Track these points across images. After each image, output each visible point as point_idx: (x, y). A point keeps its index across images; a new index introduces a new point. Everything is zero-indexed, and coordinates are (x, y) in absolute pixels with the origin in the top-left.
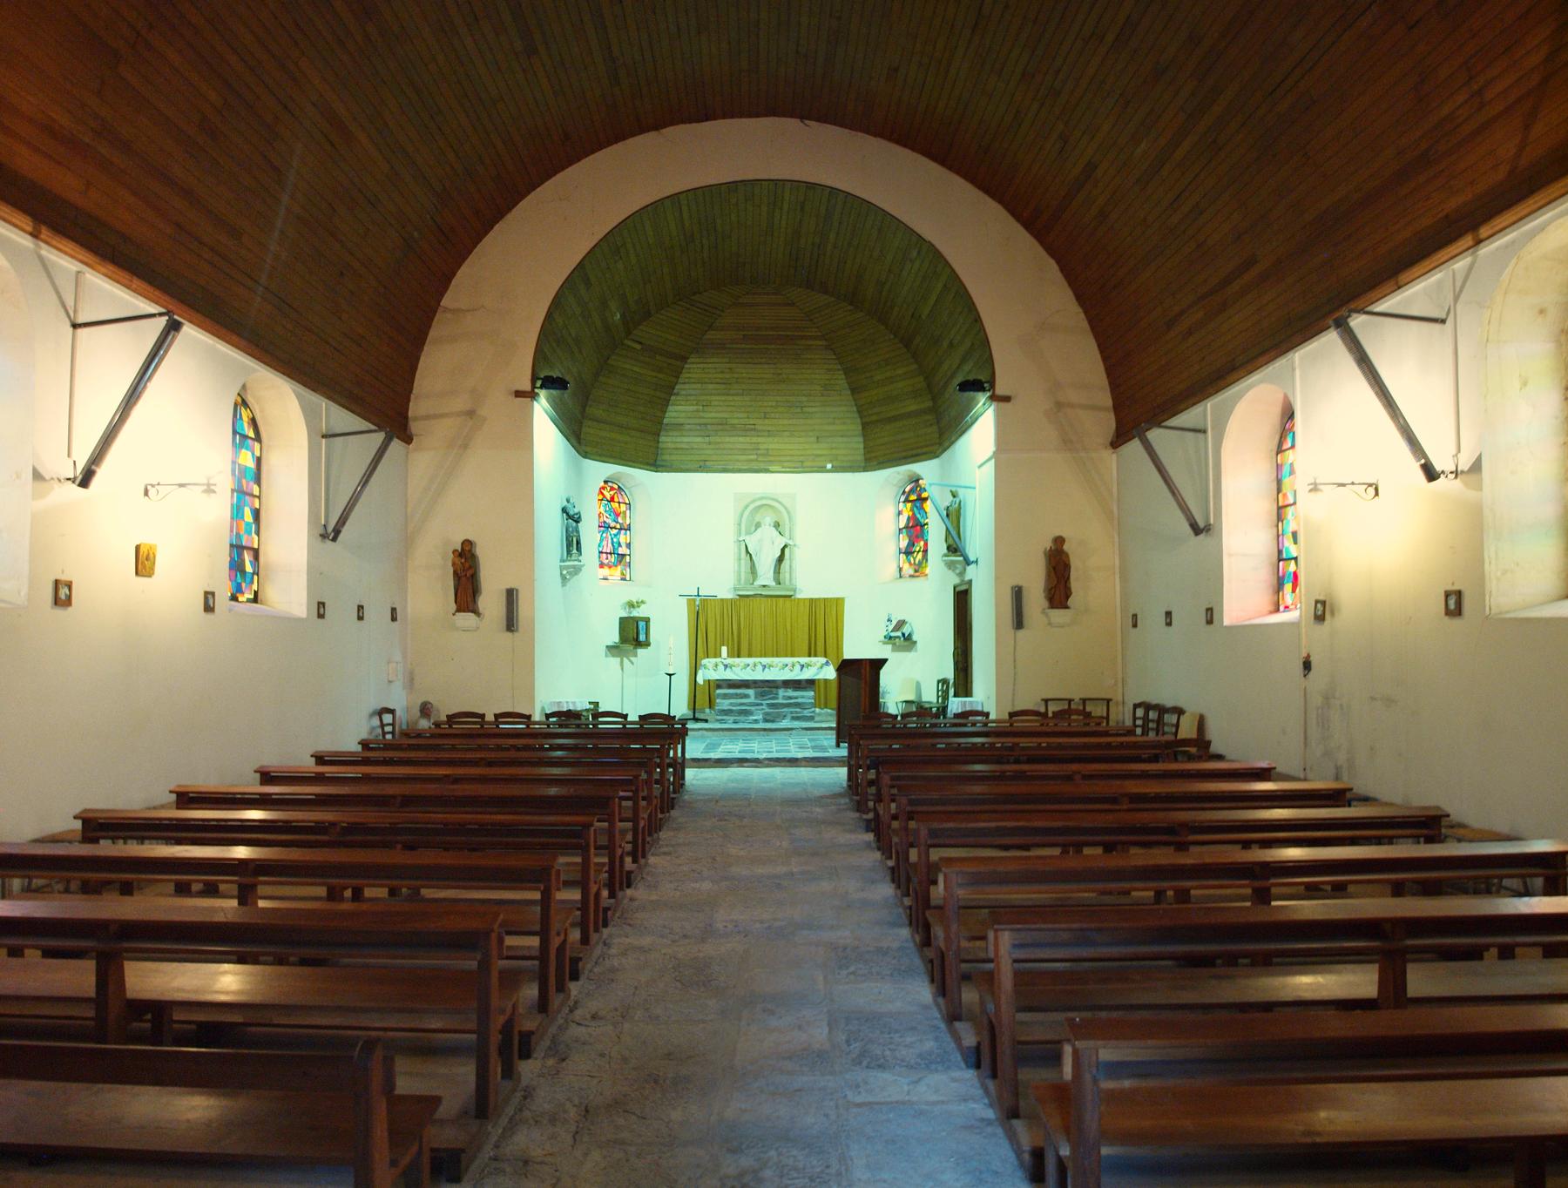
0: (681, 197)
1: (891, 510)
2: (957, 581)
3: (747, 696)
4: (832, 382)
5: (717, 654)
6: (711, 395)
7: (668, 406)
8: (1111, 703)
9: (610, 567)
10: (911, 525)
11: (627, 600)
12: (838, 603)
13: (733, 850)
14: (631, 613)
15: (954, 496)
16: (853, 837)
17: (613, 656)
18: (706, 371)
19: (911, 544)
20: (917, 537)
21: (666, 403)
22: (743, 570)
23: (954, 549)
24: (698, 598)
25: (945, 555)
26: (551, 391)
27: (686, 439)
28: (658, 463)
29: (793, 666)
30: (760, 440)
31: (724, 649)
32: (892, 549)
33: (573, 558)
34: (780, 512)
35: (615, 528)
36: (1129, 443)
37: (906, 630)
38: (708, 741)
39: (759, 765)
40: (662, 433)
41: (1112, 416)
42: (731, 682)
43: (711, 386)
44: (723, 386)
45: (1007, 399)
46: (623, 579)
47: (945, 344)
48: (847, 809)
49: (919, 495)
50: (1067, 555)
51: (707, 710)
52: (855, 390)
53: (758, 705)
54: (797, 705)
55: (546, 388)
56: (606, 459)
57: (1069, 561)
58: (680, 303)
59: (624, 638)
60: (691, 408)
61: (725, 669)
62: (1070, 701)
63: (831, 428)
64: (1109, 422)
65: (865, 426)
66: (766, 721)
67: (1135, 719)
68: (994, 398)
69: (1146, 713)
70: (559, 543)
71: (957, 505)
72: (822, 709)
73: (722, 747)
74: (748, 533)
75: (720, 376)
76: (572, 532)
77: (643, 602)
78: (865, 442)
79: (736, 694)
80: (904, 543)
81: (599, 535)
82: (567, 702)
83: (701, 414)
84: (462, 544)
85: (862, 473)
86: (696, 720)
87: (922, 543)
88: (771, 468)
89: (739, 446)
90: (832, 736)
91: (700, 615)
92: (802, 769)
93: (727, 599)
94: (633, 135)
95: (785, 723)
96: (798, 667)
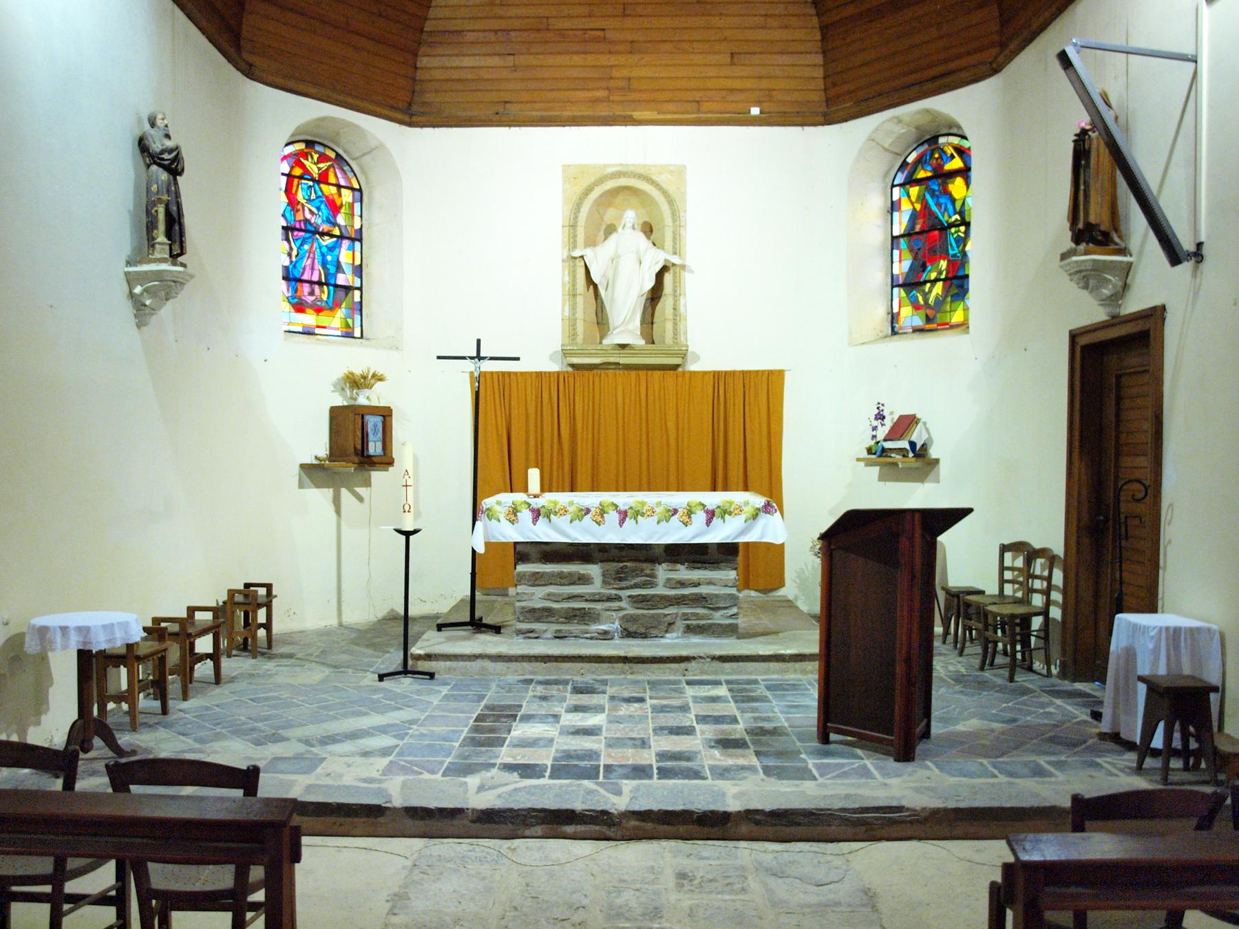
1: (876, 202)
3: (584, 580)
5: (514, 483)
9: (318, 310)
10: (918, 228)
11: (340, 373)
17: (318, 486)
19: (920, 265)
20: (932, 250)
22: (580, 314)
27: (467, 62)
28: (415, 108)
29: (690, 513)
30: (613, 60)
31: (534, 475)
32: (878, 278)
37: (918, 436)
40: (423, 50)
46: (349, 335)
53: (609, 599)
54: (700, 600)
59: (337, 452)
61: (535, 520)
63: (761, 35)
65: (825, 31)
66: (628, 634)
74: (591, 242)
77: (724, 521)
78: (825, 65)
79: (561, 575)
80: (902, 267)
88: (637, 115)
89: (575, 73)
95: (672, 643)
96: (700, 517)
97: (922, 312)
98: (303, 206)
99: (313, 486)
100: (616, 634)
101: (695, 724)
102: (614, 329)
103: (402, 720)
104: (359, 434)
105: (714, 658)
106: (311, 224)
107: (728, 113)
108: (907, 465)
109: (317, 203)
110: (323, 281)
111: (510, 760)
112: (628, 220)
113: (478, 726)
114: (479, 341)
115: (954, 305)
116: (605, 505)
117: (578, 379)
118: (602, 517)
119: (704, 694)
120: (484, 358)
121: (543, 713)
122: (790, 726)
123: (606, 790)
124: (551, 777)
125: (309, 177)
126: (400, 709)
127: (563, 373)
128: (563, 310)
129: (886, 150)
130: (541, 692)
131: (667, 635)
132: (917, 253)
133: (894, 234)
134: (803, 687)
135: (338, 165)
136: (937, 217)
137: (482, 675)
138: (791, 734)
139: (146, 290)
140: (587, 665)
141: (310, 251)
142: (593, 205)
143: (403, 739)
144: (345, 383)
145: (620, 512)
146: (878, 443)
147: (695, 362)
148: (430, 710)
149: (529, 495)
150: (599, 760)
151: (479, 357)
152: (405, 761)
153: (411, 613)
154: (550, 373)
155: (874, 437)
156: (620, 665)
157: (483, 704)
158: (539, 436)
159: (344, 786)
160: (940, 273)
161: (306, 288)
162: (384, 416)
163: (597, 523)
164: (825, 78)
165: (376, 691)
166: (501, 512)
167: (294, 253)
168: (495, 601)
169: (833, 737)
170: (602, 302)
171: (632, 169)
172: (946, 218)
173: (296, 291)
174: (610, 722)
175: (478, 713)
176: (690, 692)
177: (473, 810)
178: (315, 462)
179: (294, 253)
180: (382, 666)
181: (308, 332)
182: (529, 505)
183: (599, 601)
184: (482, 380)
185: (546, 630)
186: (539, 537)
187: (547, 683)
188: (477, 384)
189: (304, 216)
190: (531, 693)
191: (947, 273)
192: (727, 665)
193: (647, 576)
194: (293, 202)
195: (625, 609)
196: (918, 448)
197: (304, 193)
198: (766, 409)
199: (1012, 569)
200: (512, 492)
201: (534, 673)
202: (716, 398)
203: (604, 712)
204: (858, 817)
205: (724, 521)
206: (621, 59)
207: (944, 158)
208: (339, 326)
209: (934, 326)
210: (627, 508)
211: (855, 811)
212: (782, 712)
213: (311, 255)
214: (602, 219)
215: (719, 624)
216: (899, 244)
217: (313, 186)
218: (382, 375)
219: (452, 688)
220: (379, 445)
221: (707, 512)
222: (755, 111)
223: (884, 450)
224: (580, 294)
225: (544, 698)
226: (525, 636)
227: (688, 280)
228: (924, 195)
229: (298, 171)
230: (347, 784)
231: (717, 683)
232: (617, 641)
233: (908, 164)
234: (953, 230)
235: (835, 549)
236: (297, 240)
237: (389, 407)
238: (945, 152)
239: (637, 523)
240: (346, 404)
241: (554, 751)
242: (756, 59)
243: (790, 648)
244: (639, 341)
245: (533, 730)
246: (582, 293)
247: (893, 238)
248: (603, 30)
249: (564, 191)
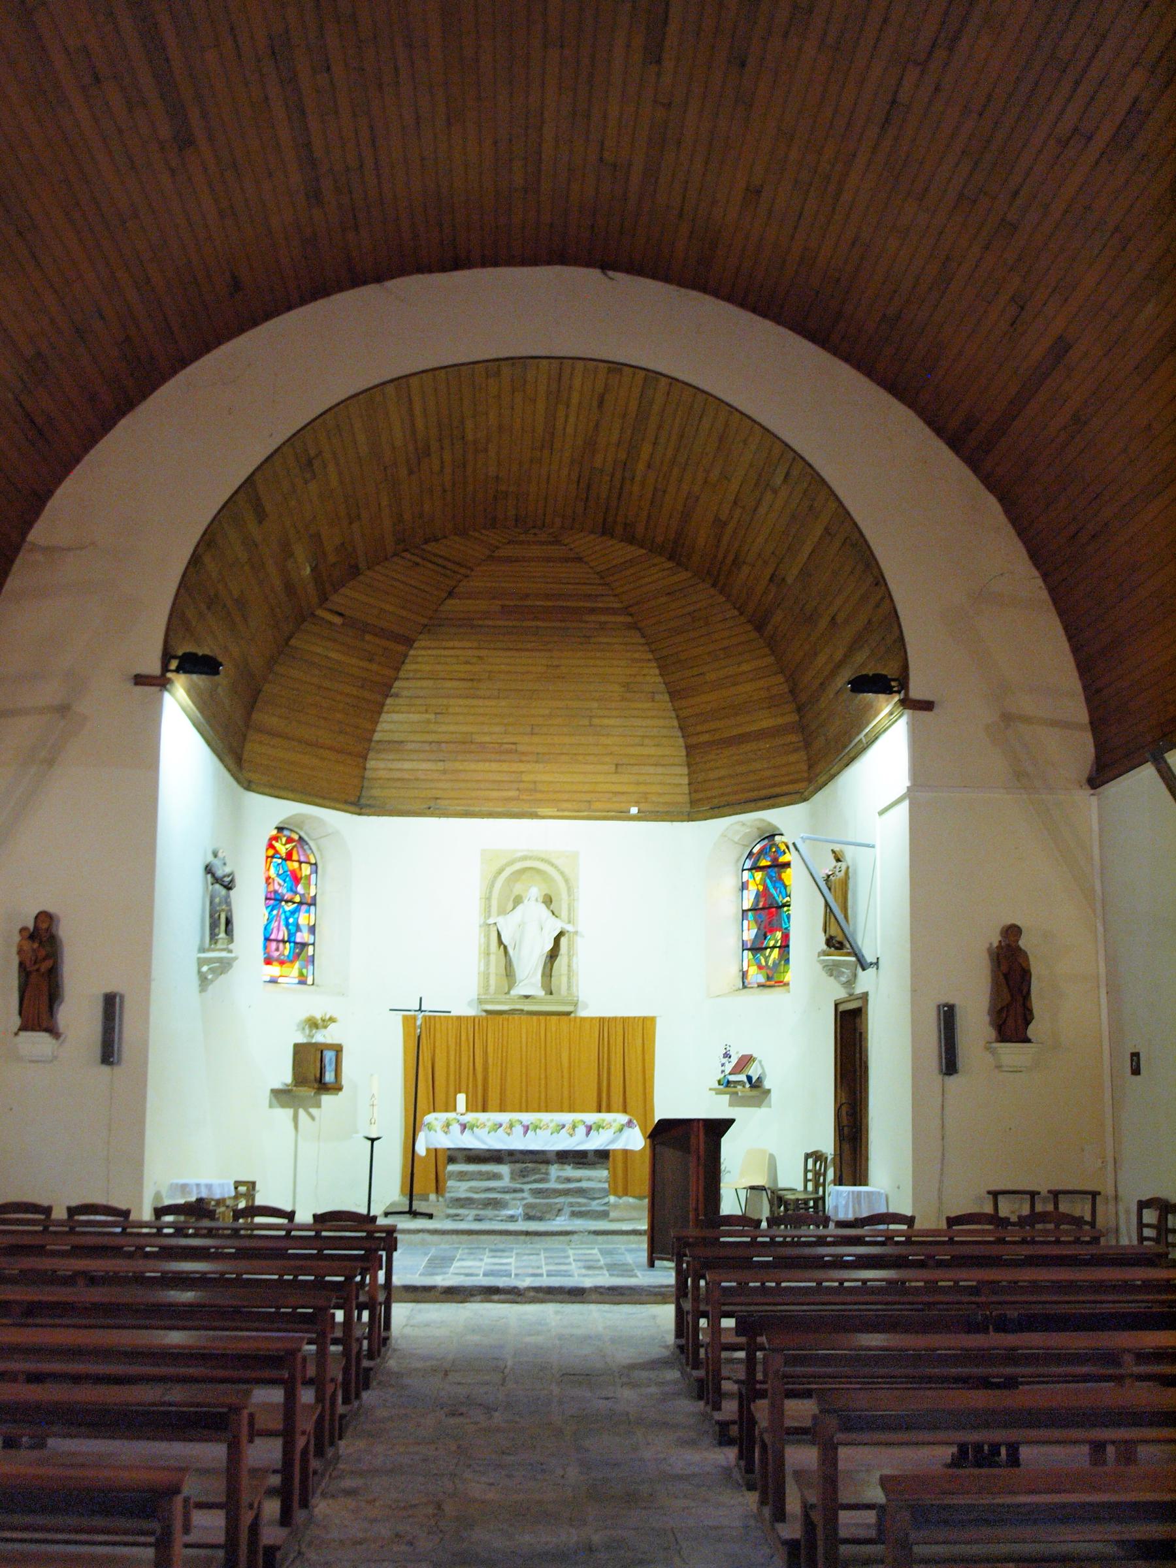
0: (414, 381)
1: (730, 882)
2: (842, 994)
3: (496, 1176)
4: (639, 679)
5: (450, 1107)
6: (448, 697)
7: (380, 713)
8: (1098, 1197)
9: (282, 963)
10: (761, 905)
11: (304, 1015)
12: (645, 1026)
13: (478, 1487)
14: (313, 1037)
15: (838, 860)
16: (697, 1457)
17: (283, 1106)
18: (443, 660)
19: (763, 934)
21: (379, 709)
22: (493, 969)
23: (838, 943)
24: (420, 1015)
25: (824, 953)
26: (194, 677)
27: (407, 765)
28: (363, 801)
29: (574, 1127)
30: (523, 767)
31: (461, 1098)
32: (731, 944)
33: (219, 946)
35: (291, 901)
36: (1137, 770)
38: (433, 1252)
39: (519, 1299)
40: (371, 755)
41: (1087, 739)
42: (471, 1153)
43: (449, 684)
44: (469, 684)
45: (926, 706)
46: (303, 982)
47: (823, 623)
48: (678, 1394)
49: (775, 860)
50: (1025, 955)
51: (433, 1197)
52: (675, 694)
53: (515, 1191)
54: (581, 1192)
55: (186, 672)
56: (282, 793)
57: (1029, 965)
58: (404, 554)
59: (299, 1078)
60: (415, 717)
61: (463, 1131)
62: (1033, 1195)
63: (640, 750)
64: (1084, 747)
65: (689, 748)
66: (528, 1218)
67: (1141, 1225)
68: (907, 703)
69: (1163, 1219)
70: (198, 928)
71: (843, 873)
72: (620, 1197)
73: (456, 1264)
74: (502, 912)
76: (220, 904)
77: (332, 1020)
78: (689, 775)
79: (480, 1173)
80: (750, 934)
81: (266, 913)
82: (198, 1185)
83: (432, 727)
84: (36, 917)
85: (685, 823)
86: (413, 1213)
87: (779, 935)
88: (541, 811)
90: (643, 1244)
91: (423, 1041)
92: (593, 1307)
93: (467, 1018)
94: (341, 289)
95: (560, 1223)
96: (581, 1130)
97: (764, 971)
98: (273, 880)
104: (318, 1064)
117: (490, 1022)
131: (558, 1218)
139: (209, 969)
140: (498, 1238)
141: (278, 915)
145: (524, 1126)
154: (467, 1017)
160: (777, 942)
164: (689, 784)
166: (438, 1126)
170: (510, 960)
181: (273, 981)
206: (529, 767)
209: (772, 983)
214: (512, 891)
215: (597, 1211)
220: (333, 1074)
222: (634, 810)
223: (728, 1082)
227: (580, 943)
242: (635, 769)
244: (541, 993)
247: (744, 911)
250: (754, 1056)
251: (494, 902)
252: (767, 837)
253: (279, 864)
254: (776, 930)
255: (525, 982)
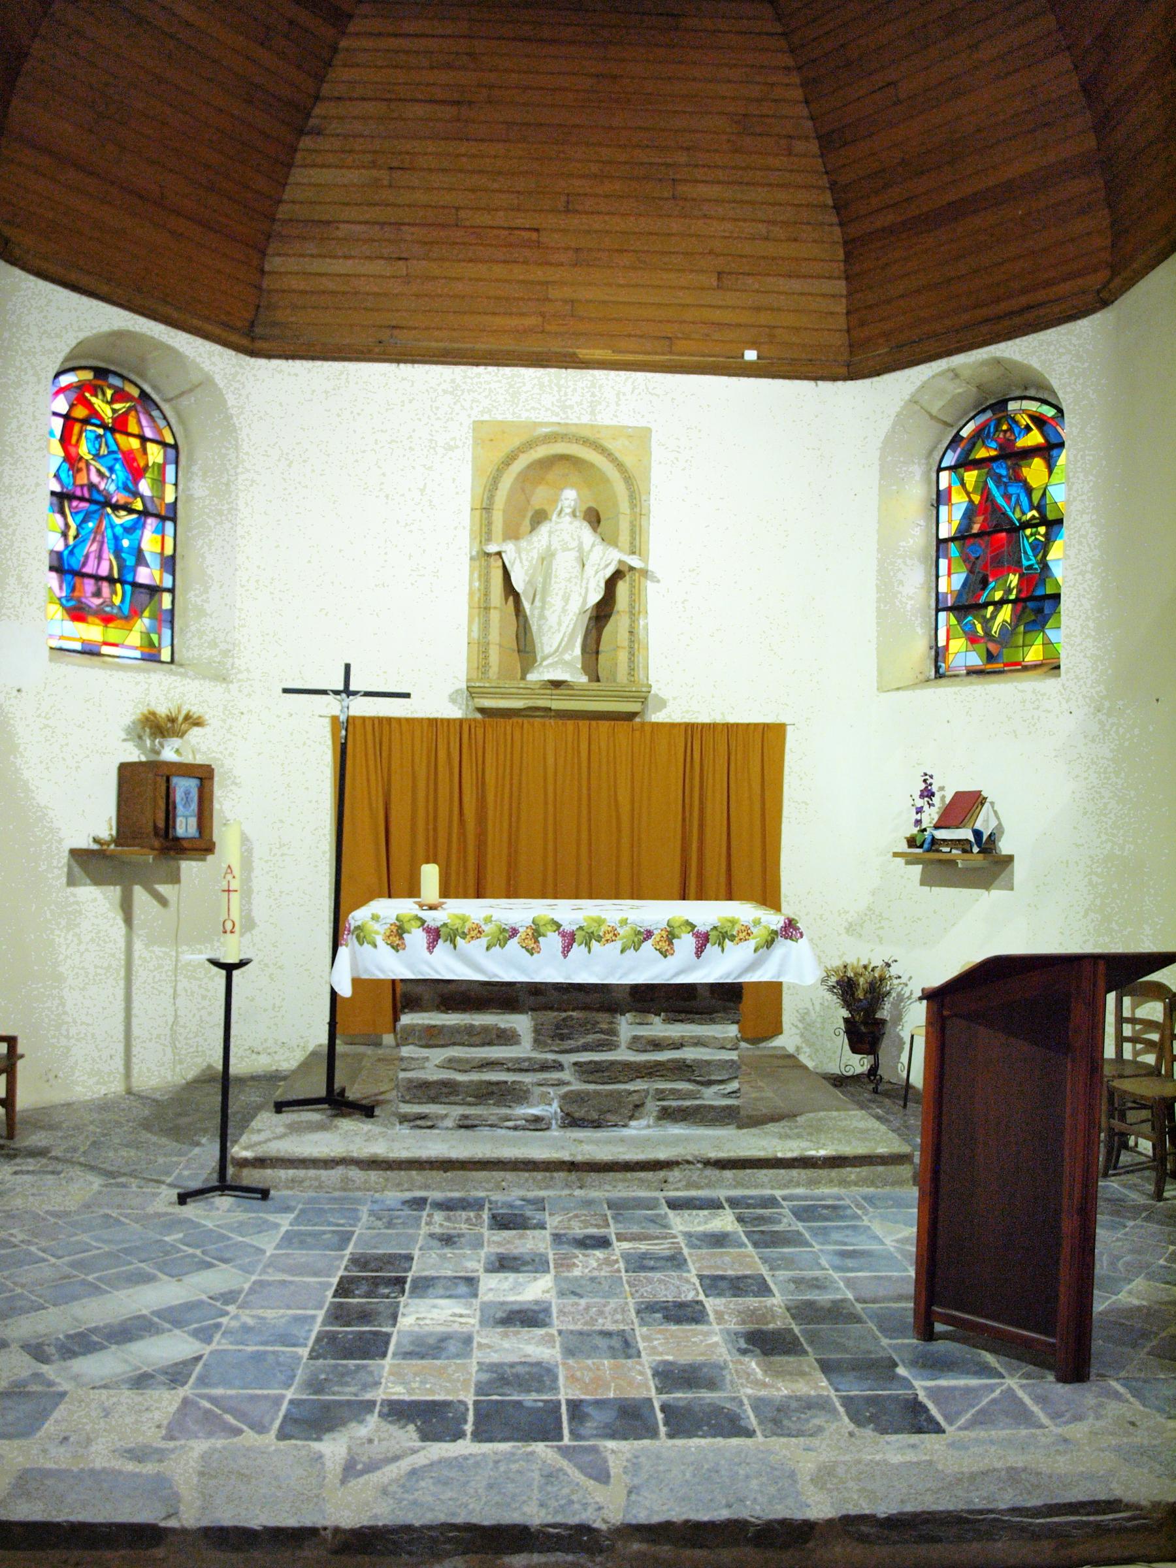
1: (916, 492)
3: (506, 1037)
9: (107, 620)
10: (976, 528)
19: (978, 580)
22: (494, 636)
28: (258, 330)
29: (671, 936)
31: (430, 874)
34: (605, 480)
37: (984, 821)
42: (448, 989)
46: (151, 656)
53: (544, 1067)
54: (682, 1069)
59: (127, 830)
61: (431, 946)
65: (852, 248)
66: (572, 1121)
74: (512, 534)
75: (445, 77)
77: (723, 950)
78: (849, 295)
79: (470, 1030)
80: (952, 582)
97: (981, 647)
98: (88, 464)
99: (88, 881)
100: (554, 1122)
101: (702, 1297)
102: (544, 658)
103: (211, 1294)
105: (708, 1163)
106: (99, 492)
107: (713, 356)
108: (970, 864)
109: (109, 461)
110: (116, 576)
111: (399, 1392)
112: (566, 503)
113: (341, 1304)
114: (348, 667)
115: (1029, 636)
116: (542, 923)
117: (489, 730)
118: (536, 941)
119: (701, 1229)
120: (355, 693)
121: (449, 1273)
122: (857, 1300)
123: (582, 1469)
124: (478, 1436)
125: (97, 422)
126: (210, 1266)
127: (466, 719)
128: (470, 631)
129: (932, 417)
130: (441, 1225)
131: (633, 1123)
132: (974, 563)
133: (941, 536)
134: (848, 1212)
135: (144, 408)
136: (1004, 514)
137: (345, 1190)
138: (865, 1317)
140: (509, 1175)
141: (97, 530)
142: (517, 479)
143: (208, 1340)
144: (143, 728)
145: (563, 935)
146: (925, 830)
147: (660, 710)
148: (260, 1267)
149: (421, 906)
150: (554, 1389)
151: (347, 691)
152: (211, 1399)
153: (233, 1070)
154: (448, 720)
155: (918, 822)
156: (562, 1175)
157: (348, 1252)
158: (431, 807)
159: (92, 1472)
160: (1009, 591)
161: (89, 586)
162: (201, 779)
163: (527, 950)
164: (848, 313)
165: (174, 1224)
166: (379, 931)
167: (72, 532)
168: (364, 1055)
169: (939, 1327)
171: (573, 430)
172: (1018, 514)
173: (73, 589)
174: (561, 1294)
175: (341, 1273)
176: (681, 1223)
177: (337, 1530)
178: (95, 847)
179: (72, 532)
180: (186, 1173)
181: (90, 651)
182: (423, 922)
183: (527, 1071)
184: (350, 728)
185: (446, 1116)
186: (437, 972)
187: (447, 1206)
188: (343, 733)
189: (89, 478)
190: (424, 1230)
191: (1019, 592)
192: (728, 1174)
193: (602, 1032)
194: (72, 460)
195: (568, 1083)
196: (985, 838)
197: (90, 445)
198: (759, 781)
199: (1133, 1021)
200: (390, 897)
201: (426, 1187)
202: (688, 765)
203: (547, 1271)
204: (1042, 1524)
205: (723, 950)
207: (1016, 430)
208: (138, 644)
209: (998, 666)
210: (574, 928)
211: (1036, 1512)
212: (837, 1268)
213: (99, 538)
215: (712, 1107)
216: (947, 549)
217: (104, 435)
218: (199, 717)
219: (296, 1219)
220: (193, 822)
221: (697, 935)
222: (751, 355)
223: (934, 841)
224: (495, 608)
225: (447, 1240)
226: (412, 1124)
228: (986, 483)
229: (80, 412)
230: (98, 1464)
231: (714, 1205)
232: (555, 1132)
233: (962, 438)
234: (1028, 532)
235: (950, 1017)
236: (77, 513)
237: (209, 766)
238: (1017, 423)
239: (589, 951)
240: (143, 759)
241: (475, 1368)
243: (823, 1146)
245: (435, 1314)
246: (498, 605)
247: (940, 542)
248: (537, 230)
249: (475, 458)
250: (984, 794)
251: (498, 517)
252: (991, 407)
253: (99, 437)
254: (1009, 570)
255: (549, 661)
